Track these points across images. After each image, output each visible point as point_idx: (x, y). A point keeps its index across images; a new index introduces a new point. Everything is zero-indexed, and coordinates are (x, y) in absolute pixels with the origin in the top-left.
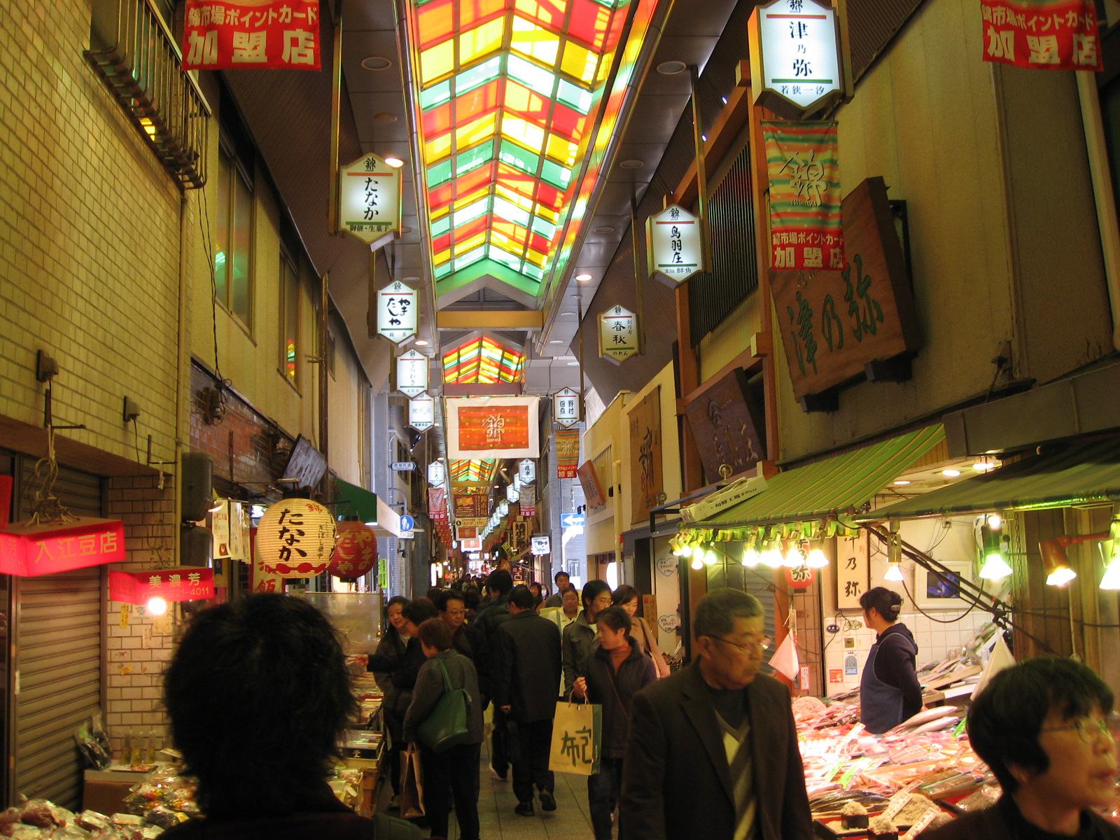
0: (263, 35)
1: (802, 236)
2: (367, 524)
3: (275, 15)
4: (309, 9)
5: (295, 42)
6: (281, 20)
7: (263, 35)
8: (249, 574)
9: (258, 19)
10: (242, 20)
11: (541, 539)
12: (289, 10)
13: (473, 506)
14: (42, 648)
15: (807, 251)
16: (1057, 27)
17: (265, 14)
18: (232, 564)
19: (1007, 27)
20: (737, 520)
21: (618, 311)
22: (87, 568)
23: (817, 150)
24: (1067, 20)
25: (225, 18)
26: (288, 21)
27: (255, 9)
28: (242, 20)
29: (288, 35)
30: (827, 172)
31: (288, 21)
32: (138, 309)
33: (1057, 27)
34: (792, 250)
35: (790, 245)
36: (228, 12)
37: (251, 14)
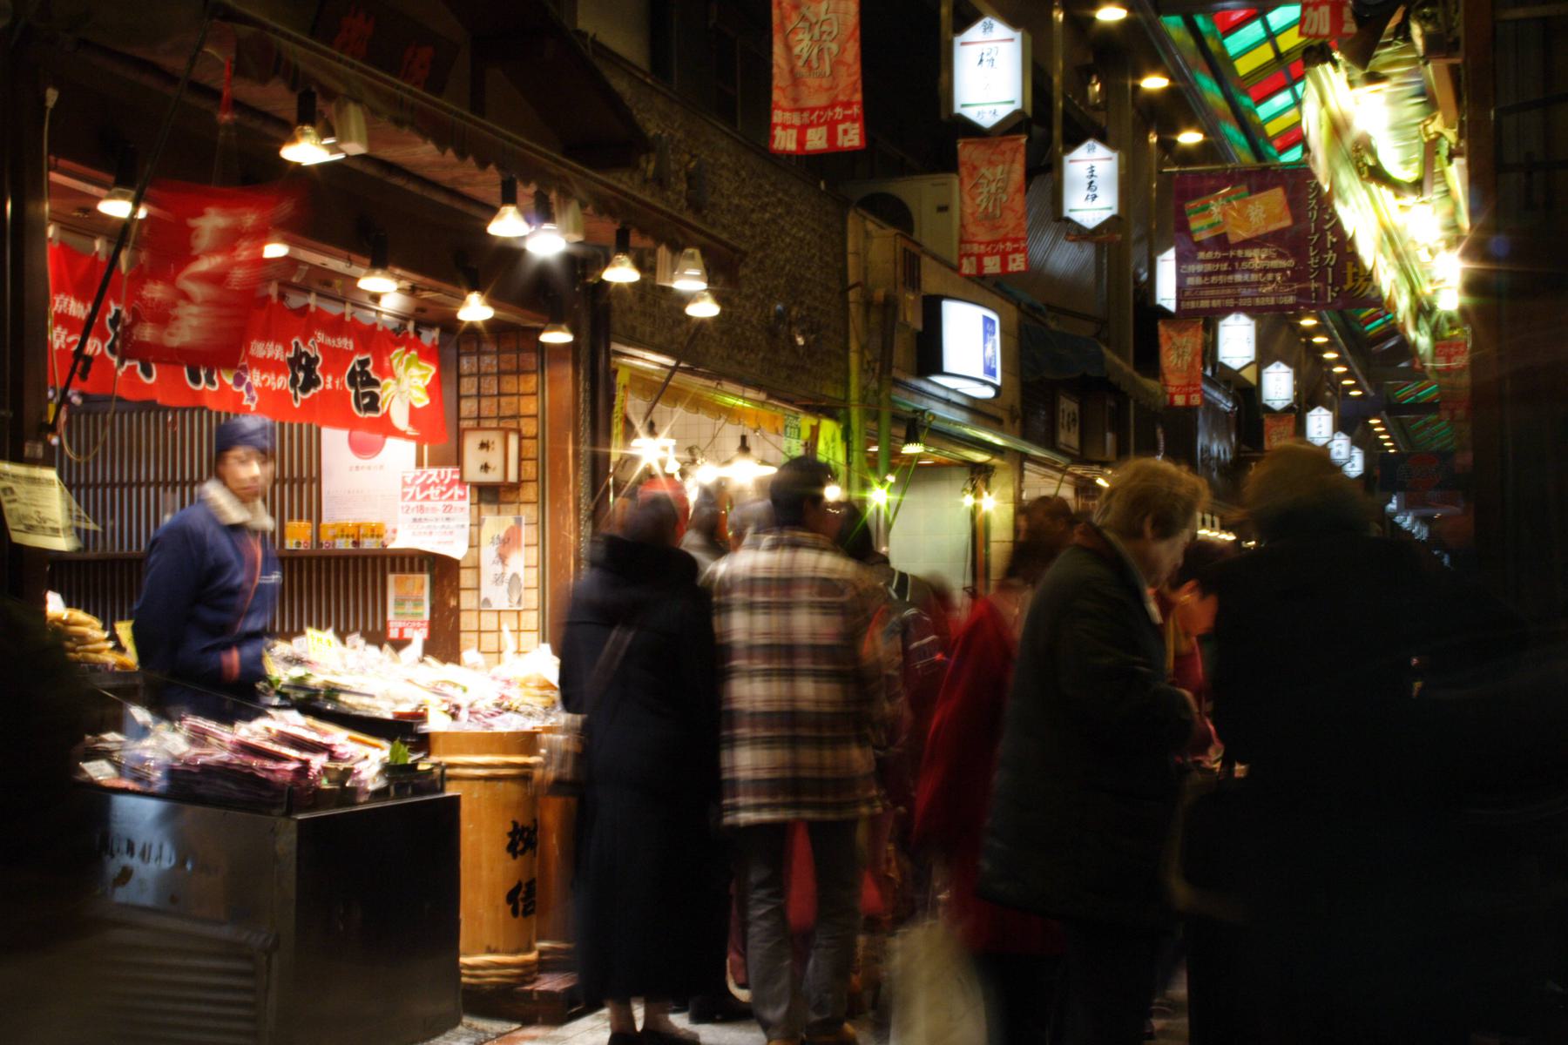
1: (806, 115)
10: (812, 118)
19: (792, 126)
24: (835, 113)
28: (812, 118)
29: (841, 128)
35: (792, 126)
37: (817, 113)
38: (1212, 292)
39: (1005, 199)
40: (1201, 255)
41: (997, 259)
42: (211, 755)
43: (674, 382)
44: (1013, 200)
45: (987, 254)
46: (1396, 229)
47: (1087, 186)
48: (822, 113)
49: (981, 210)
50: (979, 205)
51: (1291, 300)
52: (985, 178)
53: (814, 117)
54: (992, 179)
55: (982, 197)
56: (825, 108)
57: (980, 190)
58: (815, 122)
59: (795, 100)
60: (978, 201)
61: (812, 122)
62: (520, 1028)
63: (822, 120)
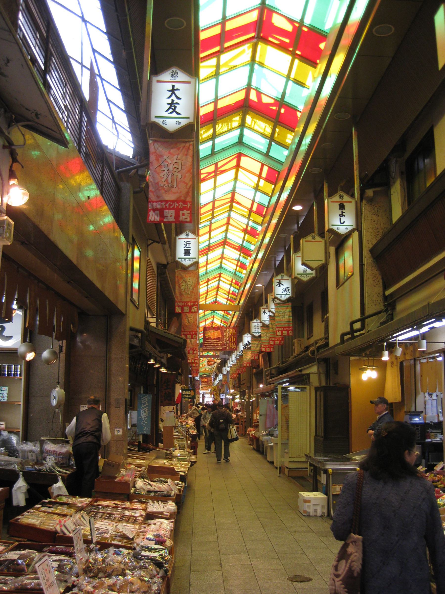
0: (173, 211)
1: (183, 303)
3: (178, 205)
4: (188, 203)
5: (183, 214)
6: (180, 207)
7: (173, 211)
8: (181, 505)
9: (172, 205)
10: (166, 205)
11: (223, 394)
12: (182, 204)
13: (207, 382)
14: (306, 326)
15: (284, 332)
16: (176, 207)
17: (174, 203)
18: (267, 179)
20: (220, 229)
21: (248, 335)
22: (384, 390)
23: (287, 309)
24: (179, 205)
25: (161, 206)
26: (182, 207)
27: (170, 201)
28: (166, 205)
29: (181, 212)
30: (289, 314)
31: (182, 207)
32: (191, 580)
33: (176, 207)
34: (280, 332)
36: (162, 204)
37: (169, 203)
38: (209, 347)
39: (179, 176)
40: (207, 340)
41: (190, 335)
42: (296, 388)
43: (236, 121)
44: (185, 177)
45: (185, 306)
46: (259, 202)
48: (171, 203)
49: (163, 180)
50: (162, 178)
51: (77, 528)
52: (167, 162)
53: (167, 205)
54: (170, 162)
55: (163, 174)
56: (173, 201)
57: (163, 169)
58: (168, 207)
59: (158, 197)
60: (161, 175)
61: (166, 207)
62: (129, 132)
63: (171, 207)
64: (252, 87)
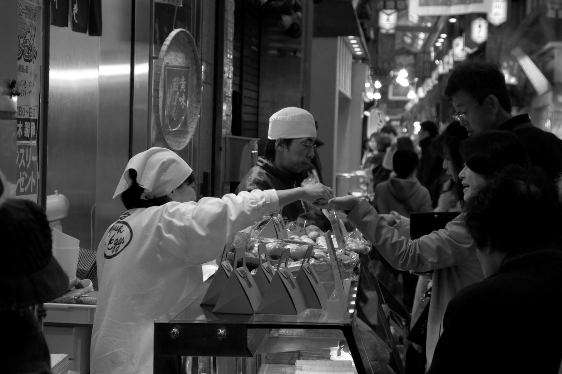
1: (28, 132)
2: (114, 197)
47: (26, 82)
64: (464, 185)
